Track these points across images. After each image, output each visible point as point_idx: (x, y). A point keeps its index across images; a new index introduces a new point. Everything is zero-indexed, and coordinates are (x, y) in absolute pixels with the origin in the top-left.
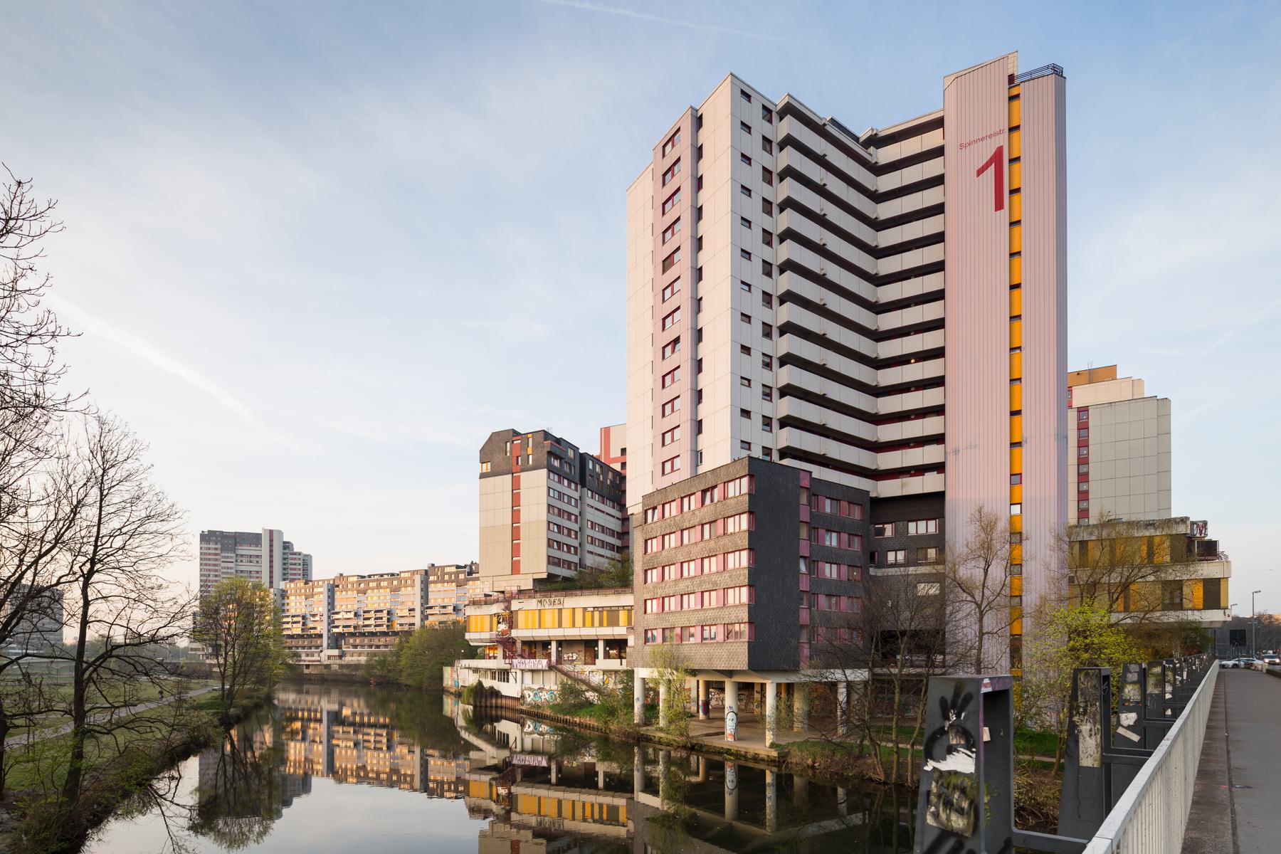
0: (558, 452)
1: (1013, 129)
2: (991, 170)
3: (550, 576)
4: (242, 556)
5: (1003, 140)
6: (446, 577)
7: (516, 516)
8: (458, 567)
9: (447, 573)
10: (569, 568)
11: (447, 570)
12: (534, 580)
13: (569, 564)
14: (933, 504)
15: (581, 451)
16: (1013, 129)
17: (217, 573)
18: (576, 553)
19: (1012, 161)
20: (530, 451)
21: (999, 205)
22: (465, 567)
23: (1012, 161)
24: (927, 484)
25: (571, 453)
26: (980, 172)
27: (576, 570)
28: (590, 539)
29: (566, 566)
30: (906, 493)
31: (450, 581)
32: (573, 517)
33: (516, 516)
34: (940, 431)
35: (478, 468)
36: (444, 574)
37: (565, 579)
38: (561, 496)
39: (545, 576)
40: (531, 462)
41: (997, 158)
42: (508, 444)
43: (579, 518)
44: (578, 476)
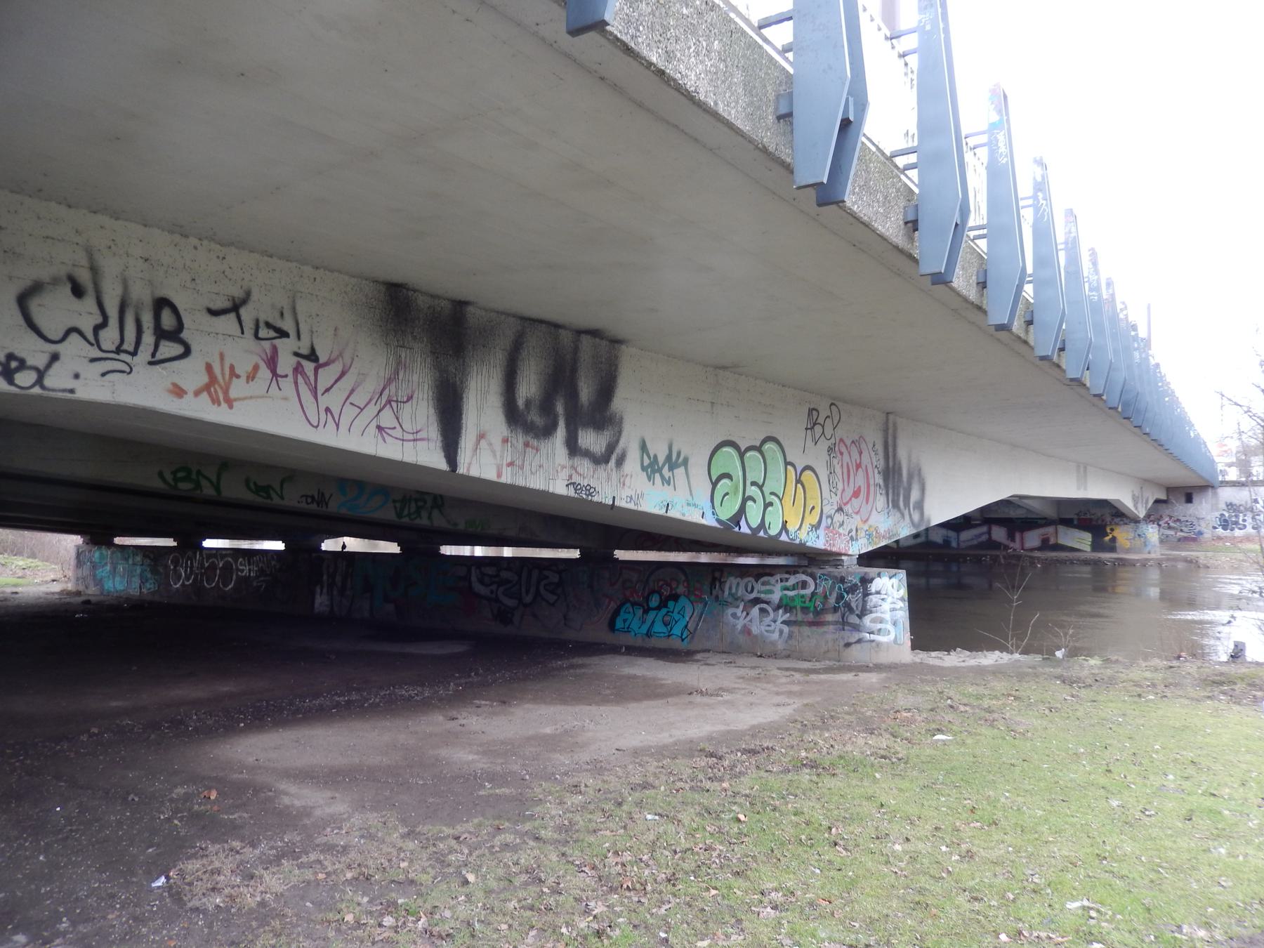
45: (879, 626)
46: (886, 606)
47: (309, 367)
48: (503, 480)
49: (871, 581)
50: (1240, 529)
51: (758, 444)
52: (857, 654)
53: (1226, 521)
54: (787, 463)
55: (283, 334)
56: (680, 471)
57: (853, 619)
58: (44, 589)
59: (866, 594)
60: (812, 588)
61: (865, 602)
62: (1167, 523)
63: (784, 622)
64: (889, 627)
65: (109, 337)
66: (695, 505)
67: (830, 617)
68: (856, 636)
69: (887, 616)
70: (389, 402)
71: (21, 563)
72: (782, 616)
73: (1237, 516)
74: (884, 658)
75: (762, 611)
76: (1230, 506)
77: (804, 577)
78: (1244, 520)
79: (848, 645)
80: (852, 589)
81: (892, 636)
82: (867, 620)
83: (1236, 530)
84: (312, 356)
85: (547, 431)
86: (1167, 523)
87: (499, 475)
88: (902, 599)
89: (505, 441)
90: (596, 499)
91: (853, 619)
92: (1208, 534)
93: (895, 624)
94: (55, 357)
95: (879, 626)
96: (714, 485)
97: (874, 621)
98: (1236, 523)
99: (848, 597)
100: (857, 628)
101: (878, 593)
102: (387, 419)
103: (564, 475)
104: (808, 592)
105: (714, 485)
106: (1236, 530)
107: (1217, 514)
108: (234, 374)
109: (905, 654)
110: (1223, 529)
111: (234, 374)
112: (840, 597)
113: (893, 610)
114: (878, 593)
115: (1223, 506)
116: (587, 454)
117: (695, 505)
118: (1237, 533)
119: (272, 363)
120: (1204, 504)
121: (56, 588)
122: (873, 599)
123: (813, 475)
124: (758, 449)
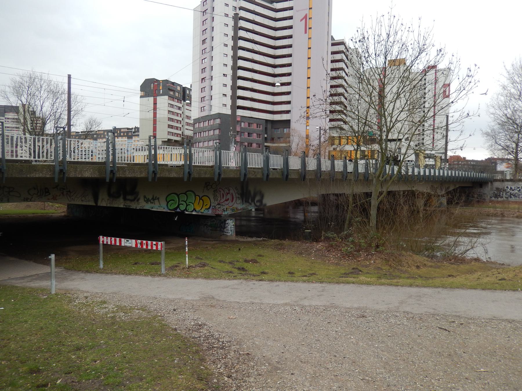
0: (173, 88)
1: (310, 8)
2: (304, 20)
3: (169, 140)
4: (8, 118)
5: (307, 12)
6: (122, 134)
7: (155, 115)
8: (128, 129)
9: (122, 132)
10: (177, 136)
11: (122, 130)
12: (162, 141)
13: (177, 135)
14: (287, 123)
15: (184, 86)
16: (310, 8)
17: (200, 152)
18: (180, 130)
19: (310, 18)
20: (161, 88)
21: (306, 32)
22: (132, 129)
23: (310, 18)
24: (284, 117)
25: (179, 88)
26: (301, 20)
27: (180, 137)
28: (187, 123)
29: (176, 135)
30: (282, 119)
31: (124, 136)
32: (179, 115)
33: (155, 115)
34: (288, 100)
35: (139, 93)
36: (121, 132)
37: (176, 141)
38: (172, 106)
39: (167, 140)
40: (161, 92)
41: (306, 17)
42: (152, 84)
43: (182, 115)
44: (182, 97)
45: (227, 231)
46: (229, 227)
47: (69, 193)
48: (108, 206)
49: (226, 221)
50: (501, 198)
51: (178, 194)
52: (223, 238)
53: (496, 195)
54: (195, 196)
55: (64, 189)
56: (156, 201)
57: (222, 230)
58: (60, 215)
59: (225, 224)
60: (215, 222)
61: (225, 226)
62: (472, 195)
63: (211, 230)
64: (230, 231)
65: (39, 194)
66: (161, 207)
67: (218, 229)
68: (223, 233)
69: (229, 229)
70: (84, 196)
71: (57, 205)
72: (210, 228)
73: (500, 193)
74: (228, 238)
75: (207, 227)
76: (498, 189)
77: (214, 219)
78: (502, 195)
79: (221, 235)
80: (222, 223)
81: (230, 233)
82: (225, 230)
83: (499, 198)
84: (69, 191)
85: (118, 197)
86: (472, 195)
87: (107, 205)
88: (233, 225)
89: (108, 199)
90: (131, 207)
91: (222, 230)
92: (488, 198)
93: (231, 231)
94: (32, 197)
95: (227, 231)
96: (168, 203)
97: (226, 230)
98: (499, 195)
99: (221, 224)
100: (223, 232)
101: (228, 224)
102: (83, 199)
103: (123, 204)
104: (215, 223)
105: (168, 203)
106: (499, 198)
107: (492, 192)
108: (57, 196)
109: (234, 237)
110: (494, 198)
111: (57, 196)
112: (220, 224)
113: (231, 228)
114: (228, 224)
115: (495, 189)
116: (128, 200)
117: (161, 207)
118: (500, 199)
119: (63, 193)
120: (486, 188)
121: (63, 214)
122: (227, 225)
123: (208, 199)
124: (185, 194)
